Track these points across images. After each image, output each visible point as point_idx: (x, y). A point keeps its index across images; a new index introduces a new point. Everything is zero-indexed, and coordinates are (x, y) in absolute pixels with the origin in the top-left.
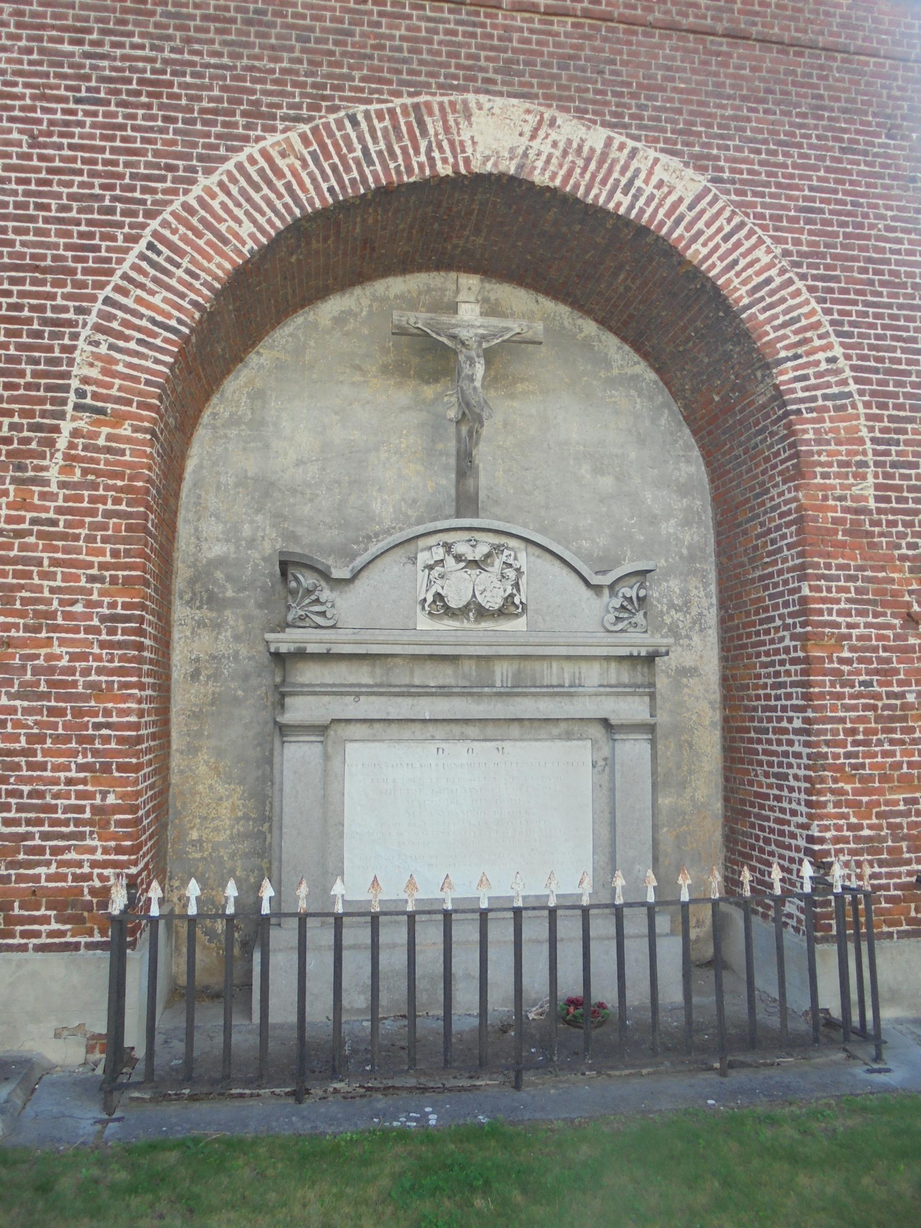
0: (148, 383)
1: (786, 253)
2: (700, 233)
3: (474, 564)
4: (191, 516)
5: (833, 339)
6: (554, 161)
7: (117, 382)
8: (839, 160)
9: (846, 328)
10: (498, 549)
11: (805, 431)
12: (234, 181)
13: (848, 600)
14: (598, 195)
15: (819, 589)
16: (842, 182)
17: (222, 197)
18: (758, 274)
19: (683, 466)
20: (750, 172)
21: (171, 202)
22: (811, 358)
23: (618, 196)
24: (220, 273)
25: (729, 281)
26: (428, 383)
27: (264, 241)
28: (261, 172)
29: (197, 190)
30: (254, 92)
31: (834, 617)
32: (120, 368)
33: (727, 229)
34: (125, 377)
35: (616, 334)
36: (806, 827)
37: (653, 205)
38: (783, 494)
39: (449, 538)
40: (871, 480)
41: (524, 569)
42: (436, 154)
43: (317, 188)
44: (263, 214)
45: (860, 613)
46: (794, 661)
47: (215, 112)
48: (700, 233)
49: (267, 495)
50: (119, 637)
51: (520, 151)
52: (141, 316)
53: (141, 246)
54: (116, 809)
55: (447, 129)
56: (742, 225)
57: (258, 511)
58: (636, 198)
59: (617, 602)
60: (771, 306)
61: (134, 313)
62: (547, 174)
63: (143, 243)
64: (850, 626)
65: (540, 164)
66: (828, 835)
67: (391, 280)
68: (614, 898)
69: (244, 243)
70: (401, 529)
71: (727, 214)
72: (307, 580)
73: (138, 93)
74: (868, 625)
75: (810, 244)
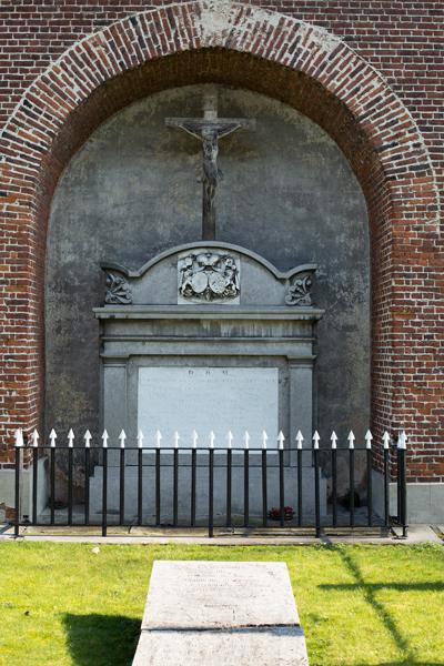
0: (27, 178)
1: (390, 81)
2: (337, 73)
3: (208, 268)
4: (54, 239)
5: (419, 132)
6: (249, 36)
7: (11, 178)
8: (429, 20)
9: (427, 125)
10: (223, 258)
11: (397, 190)
12: (69, 62)
13: (419, 289)
14: (274, 54)
15: (401, 282)
16: (430, 34)
17: (63, 72)
18: (371, 95)
19: (351, 200)
20: (370, 32)
21: (36, 77)
22: (404, 145)
23: (286, 54)
24: (63, 115)
25: (354, 101)
26: (191, 154)
27: (86, 95)
28: (83, 56)
29: (49, 69)
30: (78, 10)
31: (411, 299)
32: (12, 171)
33: (354, 69)
34: (16, 175)
35: (310, 117)
36: (391, 418)
37: (308, 58)
38: (389, 225)
39: (196, 252)
40: (438, 217)
41: (239, 269)
42: (180, 38)
43: (114, 63)
44: (85, 80)
45: (426, 296)
46: (390, 323)
47: (59, 23)
48: (337, 73)
49: (97, 225)
50: (16, 312)
51: (228, 32)
52: (22, 142)
53: (21, 103)
54: (17, 399)
55: (186, 23)
56: (364, 65)
57: (92, 235)
58: (297, 55)
59: (293, 288)
60: (379, 115)
61: (21, 163)
62: (245, 44)
63: (22, 101)
64: (419, 304)
65: (240, 39)
66: (402, 422)
67: (168, 91)
68: (279, 445)
69: (75, 98)
70: (176, 245)
71: (354, 59)
72: (115, 278)
73: (17, 16)
74: (431, 303)
75: (406, 74)
